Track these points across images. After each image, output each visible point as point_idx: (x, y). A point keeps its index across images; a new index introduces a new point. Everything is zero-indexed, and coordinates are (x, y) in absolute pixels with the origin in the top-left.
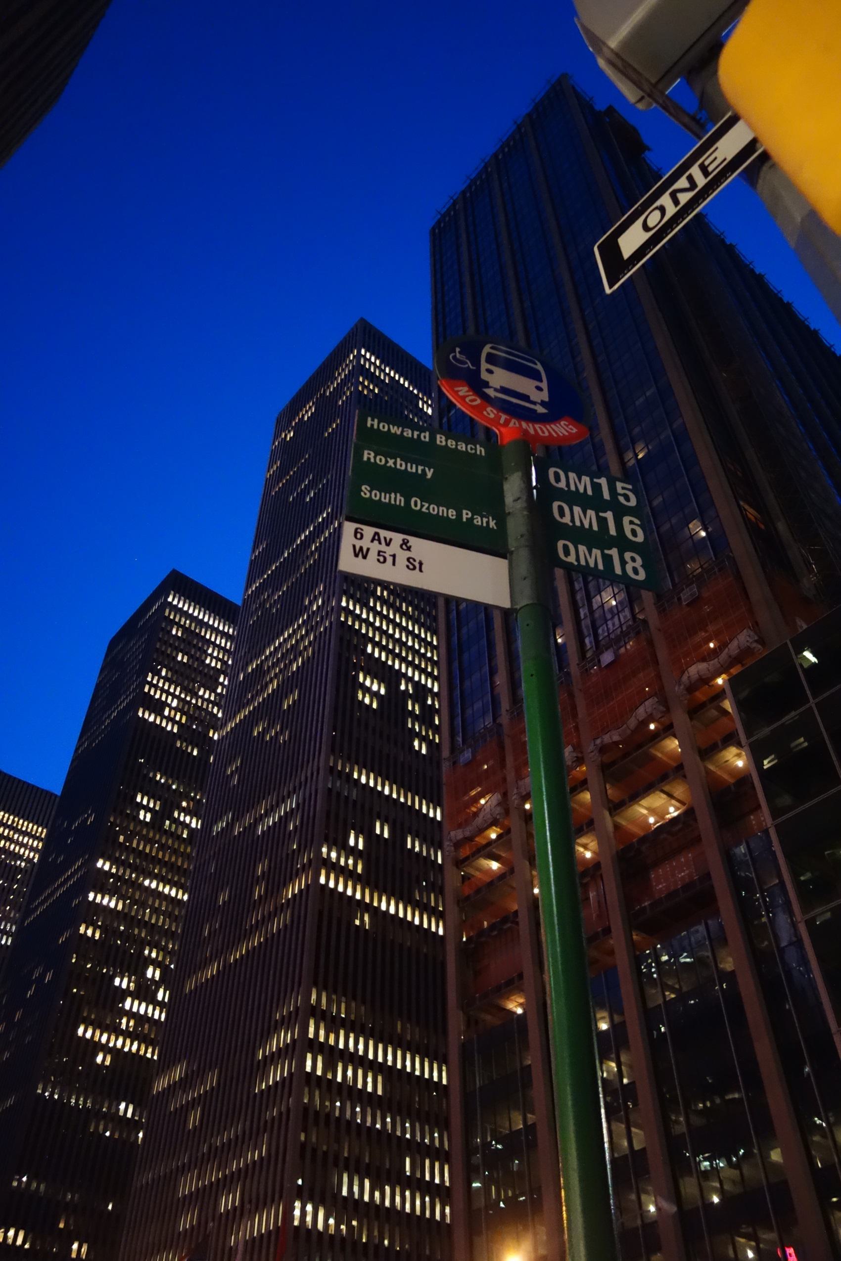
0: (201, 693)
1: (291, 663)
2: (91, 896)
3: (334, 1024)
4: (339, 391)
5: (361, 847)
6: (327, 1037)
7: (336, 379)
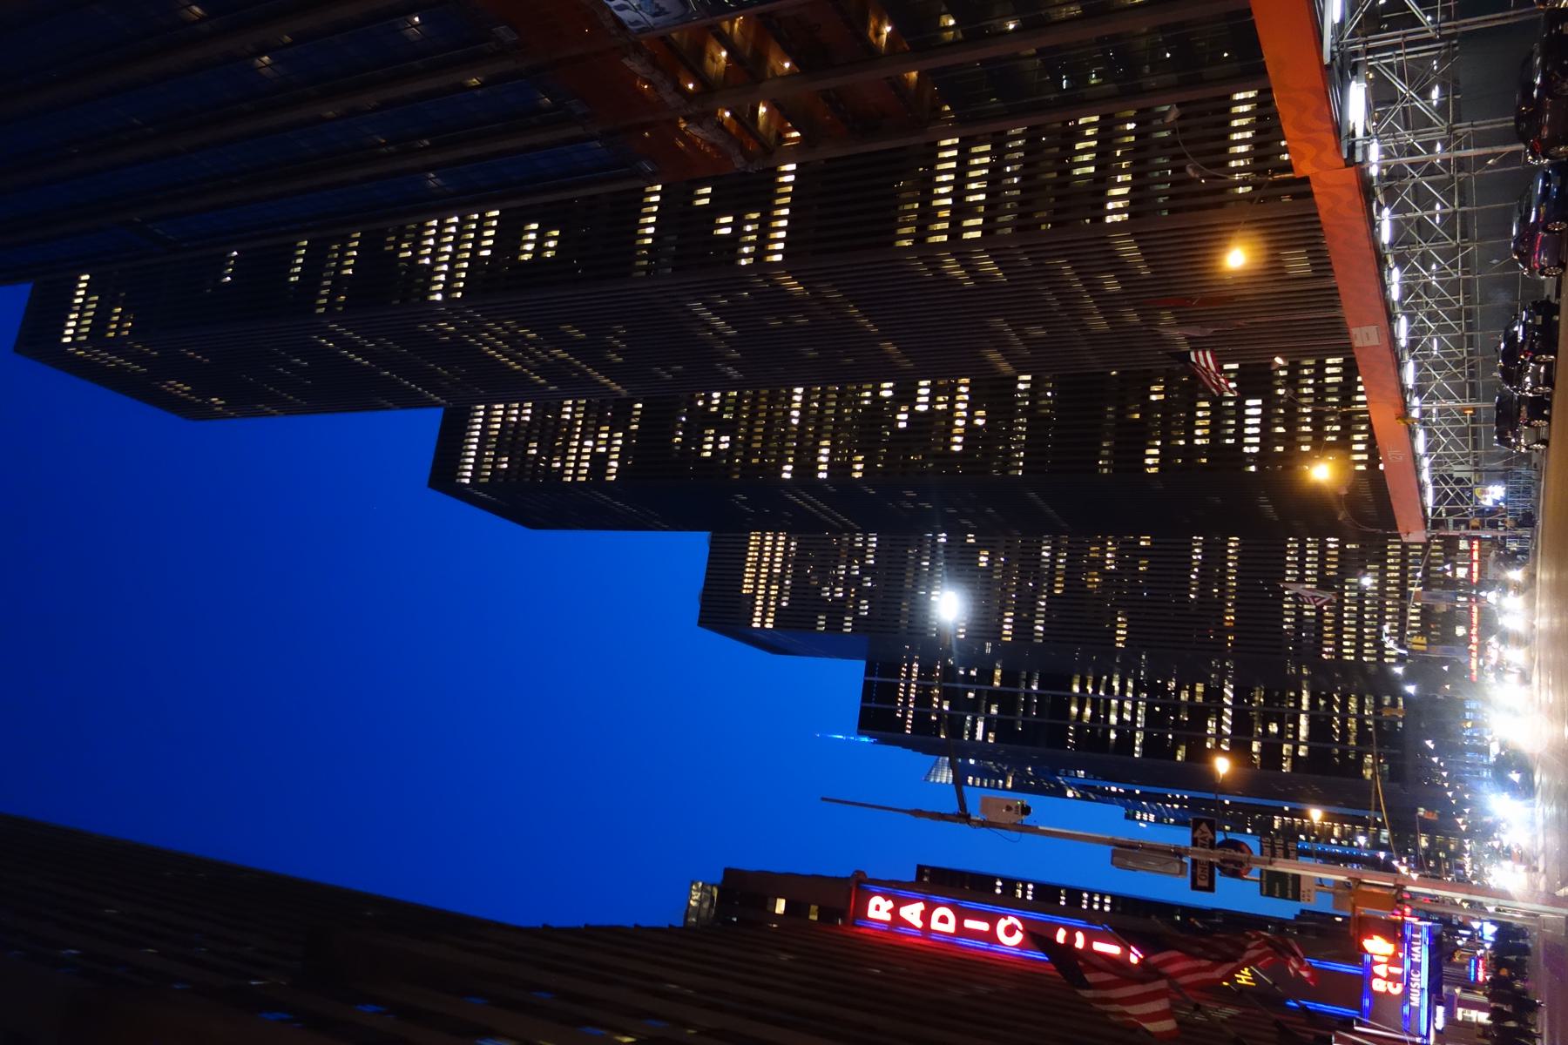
0: (568, 417)
1: (529, 340)
2: (822, 475)
3: (928, 215)
4: (139, 358)
5: (729, 219)
6: (944, 219)
7: (119, 365)
